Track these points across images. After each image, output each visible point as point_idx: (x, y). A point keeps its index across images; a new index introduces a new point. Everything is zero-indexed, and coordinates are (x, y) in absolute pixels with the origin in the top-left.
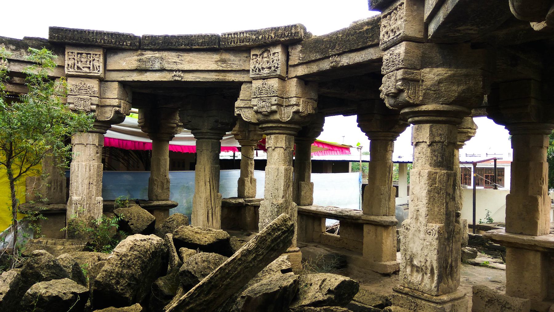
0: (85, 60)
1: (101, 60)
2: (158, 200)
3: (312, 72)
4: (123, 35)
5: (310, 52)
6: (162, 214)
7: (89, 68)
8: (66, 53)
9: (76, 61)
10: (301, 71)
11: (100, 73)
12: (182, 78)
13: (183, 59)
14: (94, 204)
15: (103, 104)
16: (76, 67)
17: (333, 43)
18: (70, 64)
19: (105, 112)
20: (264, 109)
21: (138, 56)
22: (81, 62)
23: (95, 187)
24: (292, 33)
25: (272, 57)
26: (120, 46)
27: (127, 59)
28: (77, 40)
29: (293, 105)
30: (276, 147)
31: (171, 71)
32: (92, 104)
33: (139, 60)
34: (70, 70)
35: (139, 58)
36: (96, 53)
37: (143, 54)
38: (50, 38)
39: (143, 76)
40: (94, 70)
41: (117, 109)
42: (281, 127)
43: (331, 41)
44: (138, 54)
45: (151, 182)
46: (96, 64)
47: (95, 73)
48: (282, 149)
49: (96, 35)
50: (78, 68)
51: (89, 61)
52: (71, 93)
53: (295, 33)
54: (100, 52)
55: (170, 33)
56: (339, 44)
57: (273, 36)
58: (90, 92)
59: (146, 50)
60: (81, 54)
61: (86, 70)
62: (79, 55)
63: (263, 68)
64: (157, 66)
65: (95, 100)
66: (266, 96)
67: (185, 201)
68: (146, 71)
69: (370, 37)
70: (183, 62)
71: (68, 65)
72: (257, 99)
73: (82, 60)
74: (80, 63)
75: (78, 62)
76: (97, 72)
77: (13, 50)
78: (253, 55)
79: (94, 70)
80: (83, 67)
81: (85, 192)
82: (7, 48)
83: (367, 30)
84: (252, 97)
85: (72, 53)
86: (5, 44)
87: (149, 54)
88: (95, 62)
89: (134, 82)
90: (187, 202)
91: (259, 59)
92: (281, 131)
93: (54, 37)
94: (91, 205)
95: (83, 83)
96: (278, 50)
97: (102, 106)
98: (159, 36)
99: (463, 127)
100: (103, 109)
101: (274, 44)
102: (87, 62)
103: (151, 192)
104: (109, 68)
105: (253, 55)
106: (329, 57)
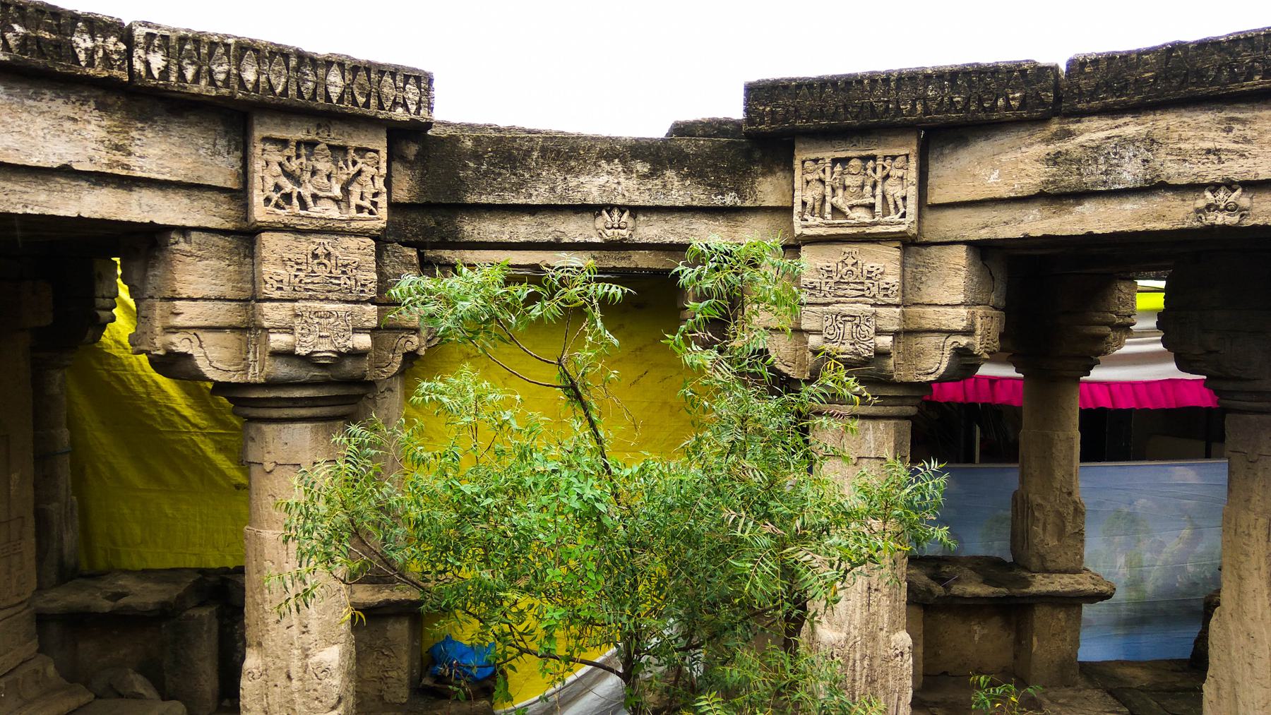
0: (858, 180)
1: (912, 175)
2: (1046, 571)
4: (993, 71)
6: (1062, 615)
7: (871, 207)
8: (797, 164)
9: (828, 189)
11: (907, 224)
12: (1243, 212)
13: (1249, 134)
14: (886, 660)
15: (912, 326)
16: (828, 208)
18: (810, 201)
19: (920, 353)
21: (1048, 141)
22: (845, 188)
23: (885, 602)
26: (982, 115)
27: (1004, 158)
28: (835, 115)
31: (1195, 188)
32: (879, 332)
33: (1054, 159)
34: (811, 220)
35: (1052, 148)
36: (895, 152)
37: (1069, 134)
38: (749, 120)
39: (1068, 218)
40: (886, 212)
41: (963, 341)
44: (1047, 133)
45: (1022, 509)
46: (894, 190)
47: (891, 224)
49: (898, 88)
50: (836, 210)
51: (869, 182)
52: (813, 300)
54: (907, 148)
55: (1192, 34)
58: (875, 290)
59: (1080, 115)
60: (845, 161)
61: (861, 215)
62: (838, 168)
64: (1130, 173)
65: (891, 318)
67: (1121, 560)
68: (1081, 195)
70: (1254, 149)
71: (804, 204)
73: (849, 181)
74: (840, 192)
75: (833, 190)
76: (896, 218)
77: (645, 176)
79: (886, 212)
80: (851, 207)
81: (857, 619)
82: (628, 171)
85: (816, 161)
86: (623, 161)
87: (1094, 131)
88: (889, 182)
89: (1027, 239)
90: (1129, 565)
93: (761, 115)
94: (877, 662)
95: (850, 261)
97: (909, 333)
98: (1140, 53)
100: (913, 340)
102: (862, 187)
103: (1020, 538)
104: (936, 197)
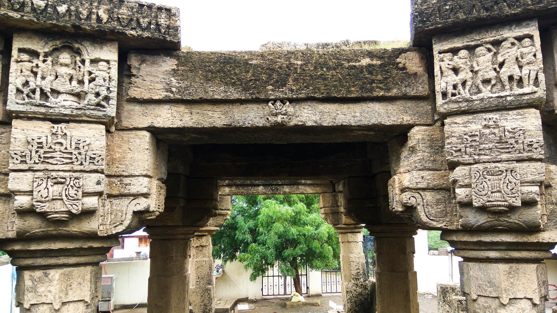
3: (206, 125)
5: (208, 80)
10: (168, 118)
17: (279, 74)
20: (59, 206)
24: (158, 25)
25: (88, 66)
29: (136, 196)
30: (64, 304)
42: (91, 248)
43: (273, 70)
48: (81, 306)
53: (168, 27)
56: (295, 80)
57: (105, 17)
63: (56, 92)
66: (67, 167)
69: (380, 82)
72: (29, 175)
78: (21, 50)
83: (370, 65)
84: (11, 166)
91: (45, 67)
92: (82, 260)
96: (110, 54)
99: (221, 207)
101: (100, 37)
105: (21, 50)
106: (266, 101)
